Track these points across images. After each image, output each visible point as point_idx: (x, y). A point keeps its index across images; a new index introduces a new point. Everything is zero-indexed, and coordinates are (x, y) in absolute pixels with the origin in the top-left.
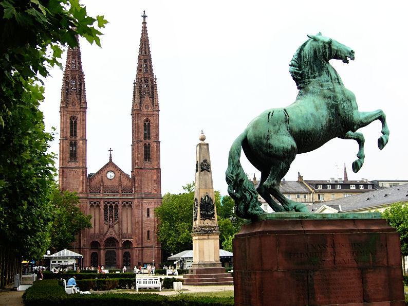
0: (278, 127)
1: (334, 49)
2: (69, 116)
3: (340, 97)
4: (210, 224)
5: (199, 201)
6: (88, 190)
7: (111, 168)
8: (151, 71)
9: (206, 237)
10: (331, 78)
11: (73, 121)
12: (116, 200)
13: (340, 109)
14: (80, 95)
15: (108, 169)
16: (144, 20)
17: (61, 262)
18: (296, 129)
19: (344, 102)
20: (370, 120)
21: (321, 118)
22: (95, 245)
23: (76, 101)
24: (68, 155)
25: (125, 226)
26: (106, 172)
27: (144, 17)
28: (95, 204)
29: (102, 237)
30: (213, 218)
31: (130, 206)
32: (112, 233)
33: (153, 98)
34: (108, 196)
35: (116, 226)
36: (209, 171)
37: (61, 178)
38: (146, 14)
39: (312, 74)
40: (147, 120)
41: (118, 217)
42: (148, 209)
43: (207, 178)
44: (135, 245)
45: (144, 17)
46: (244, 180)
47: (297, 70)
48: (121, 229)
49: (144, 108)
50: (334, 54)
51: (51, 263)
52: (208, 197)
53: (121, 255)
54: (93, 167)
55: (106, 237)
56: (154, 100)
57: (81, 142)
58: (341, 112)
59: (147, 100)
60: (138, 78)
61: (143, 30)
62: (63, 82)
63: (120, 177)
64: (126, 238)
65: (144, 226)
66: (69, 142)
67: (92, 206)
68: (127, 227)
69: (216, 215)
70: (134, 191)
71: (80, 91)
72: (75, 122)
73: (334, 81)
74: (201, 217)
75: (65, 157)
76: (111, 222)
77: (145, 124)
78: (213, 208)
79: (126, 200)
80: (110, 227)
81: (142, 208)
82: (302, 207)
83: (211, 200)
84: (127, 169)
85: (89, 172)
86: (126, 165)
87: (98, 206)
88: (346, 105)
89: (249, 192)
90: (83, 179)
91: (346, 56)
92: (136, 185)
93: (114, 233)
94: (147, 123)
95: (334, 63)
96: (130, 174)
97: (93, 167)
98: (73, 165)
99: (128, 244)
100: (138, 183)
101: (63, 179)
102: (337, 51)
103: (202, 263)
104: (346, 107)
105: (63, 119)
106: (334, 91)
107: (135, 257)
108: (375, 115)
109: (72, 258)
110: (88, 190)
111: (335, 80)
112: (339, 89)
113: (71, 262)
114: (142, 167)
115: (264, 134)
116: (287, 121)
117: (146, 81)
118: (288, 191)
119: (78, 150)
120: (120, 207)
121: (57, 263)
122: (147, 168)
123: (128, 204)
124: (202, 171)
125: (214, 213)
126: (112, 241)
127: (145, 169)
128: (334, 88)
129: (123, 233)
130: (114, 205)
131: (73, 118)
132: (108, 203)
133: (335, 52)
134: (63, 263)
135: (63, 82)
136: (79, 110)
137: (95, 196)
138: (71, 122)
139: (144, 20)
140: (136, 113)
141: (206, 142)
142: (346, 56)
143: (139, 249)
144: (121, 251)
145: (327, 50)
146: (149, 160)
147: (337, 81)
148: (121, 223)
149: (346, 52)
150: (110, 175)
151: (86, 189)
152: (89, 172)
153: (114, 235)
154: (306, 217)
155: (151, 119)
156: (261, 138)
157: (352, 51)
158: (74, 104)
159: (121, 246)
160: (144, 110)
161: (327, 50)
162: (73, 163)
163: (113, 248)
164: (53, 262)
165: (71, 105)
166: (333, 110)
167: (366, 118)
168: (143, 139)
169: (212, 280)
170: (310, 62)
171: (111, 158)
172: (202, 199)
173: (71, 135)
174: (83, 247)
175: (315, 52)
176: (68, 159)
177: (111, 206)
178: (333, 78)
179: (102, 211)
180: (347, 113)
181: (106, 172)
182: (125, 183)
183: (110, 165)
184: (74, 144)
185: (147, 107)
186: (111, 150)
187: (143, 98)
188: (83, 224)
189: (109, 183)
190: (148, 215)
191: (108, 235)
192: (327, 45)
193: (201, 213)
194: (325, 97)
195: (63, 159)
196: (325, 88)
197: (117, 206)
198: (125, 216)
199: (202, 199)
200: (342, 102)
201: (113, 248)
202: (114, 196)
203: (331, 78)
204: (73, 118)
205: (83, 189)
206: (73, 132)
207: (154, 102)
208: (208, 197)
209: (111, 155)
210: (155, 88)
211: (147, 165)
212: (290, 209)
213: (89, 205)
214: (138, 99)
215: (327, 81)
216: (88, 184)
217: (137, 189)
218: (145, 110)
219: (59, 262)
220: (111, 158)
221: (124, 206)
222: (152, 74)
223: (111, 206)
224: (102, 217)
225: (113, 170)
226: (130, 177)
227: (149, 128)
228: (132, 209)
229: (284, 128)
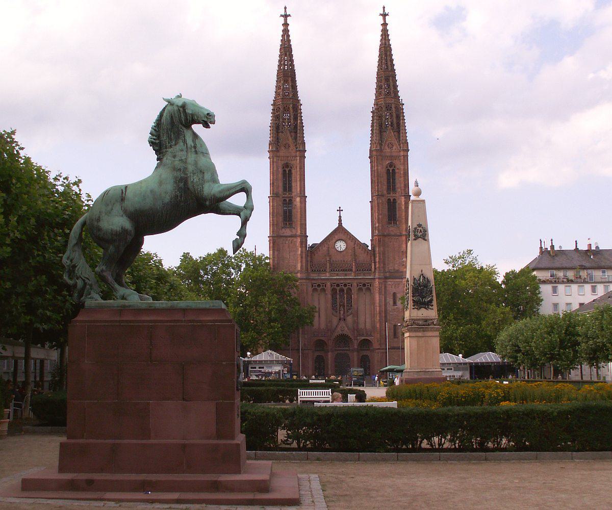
0: (110, 207)
1: (189, 114)
2: (281, 163)
3: (191, 168)
5: (411, 283)
6: (309, 267)
7: (341, 235)
8: (396, 92)
9: (420, 334)
10: (187, 147)
11: (287, 170)
12: (349, 282)
13: (189, 183)
14: (296, 132)
15: (336, 237)
16: (384, 19)
17: (263, 368)
18: (131, 209)
19: (194, 174)
20: (228, 193)
21: (163, 195)
22: (320, 344)
23: (290, 141)
24: (281, 219)
25: (361, 319)
26: (334, 241)
27: (384, 15)
28: (319, 287)
29: (329, 333)
30: (430, 307)
31: (369, 289)
32: (344, 328)
33: (399, 132)
34: (337, 275)
35: (349, 319)
36: (426, 240)
37: (271, 252)
38: (386, 12)
39: (169, 143)
40: (391, 165)
41: (351, 306)
42: (394, 294)
44: (376, 345)
45: (384, 15)
46: (76, 267)
47: (154, 139)
48: (356, 322)
49: (386, 147)
50: (189, 118)
51: (250, 369)
53: (356, 359)
54: (316, 234)
55: (336, 334)
56: (401, 135)
57: (298, 199)
58: (190, 185)
59: (390, 134)
60: (377, 105)
61: (382, 35)
62: (271, 115)
64: (363, 335)
65: (388, 317)
67: (315, 290)
68: (365, 320)
69: (434, 303)
70: (373, 267)
71: (296, 127)
72: (290, 171)
73: (189, 150)
75: (277, 222)
76: (342, 312)
78: (431, 293)
79: (362, 281)
80: (340, 319)
81: (385, 292)
82: (129, 295)
83: (428, 281)
84: (364, 234)
85: (310, 242)
86: (363, 233)
87: (324, 290)
88: (195, 179)
89: (82, 278)
90: (302, 252)
91: (207, 121)
92: (377, 259)
93: (346, 329)
94: (287, 170)
95: (197, 128)
96: (369, 244)
97: (316, 234)
98: (288, 232)
99: (366, 343)
100: (379, 257)
101: (273, 253)
102: (192, 115)
104: (195, 180)
105: (273, 168)
106: (186, 162)
107: (376, 362)
108: (235, 187)
109: (278, 362)
110: (309, 267)
111: (191, 149)
112: (193, 159)
113: (277, 368)
114: (385, 234)
115: (96, 215)
116: (123, 199)
117: (388, 108)
118: (603, 264)
119: (294, 211)
120: (354, 290)
121: (257, 369)
122: (393, 233)
123: (366, 287)
124: (415, 239)
125: (431, 301)
126: (343, 339)
127: (389, 235)
128: (186, 159)
129: (360, 328)
130: (338, 288)
131: (286, 165)
132: (338, 285)
133: (191, 116)
134: (266, 370)
135: (271, 115)
136: (294, 154)
137: (319, 276)
138: (285, 171)
139: (384, 19)
140: (376, 155)
141: (421, 197)
142: (207, 121)
143: (382, 351)
144: (355, 354)
145: (182, 114)
146: (395, 223)
147: (193, 150)
148: (356, 315)
149: (202, 115)
150: (341, 246)
151: (307, 265)
152: (310, 242)
153: (347, 332)
154: (130, 306)
155: (396, 162)
156: (93, 220)
157: (208, 114)
158: (287, 146)
159: (356, 347)
160: (387, 150)
161: (182, 114)
163: (347, 350)
164: (252, 368)
165: (283, 148)
166: (182, 185)
167: (220, 192)
168: (385, 192)
170: (167, 129)
171: (340, 220)
172: (414, 279)
173: (285, 190)
175: (172, 117)
176: (281, 224)
178: (189, 146)
179: (330, 296)
180: (196, 187)
181: (334, 241)
182: (362, 257)
183: (340, 232)
184: (288, 202)
185: (391, 146)
186: (340, 210)
187: (384, 134)
188: (304, 319)
190: (395, 303)
191: (339, 332)
192: (181, 109)
194: (175, 169)
195: (273, 225)
196: (177, 159)
198: (361, 302)
199: (414, 279)
200: (192, 175)
201: (347, 350)
202: (346, 275)
203: (187, 147)
204: (286, 165)
205: (302, 266)
206: (288, 187)
207: (401, 138)
209: (340, 217)
210: (402, 118)
211: (392, 229)
212: (118, 297)
213: (310, 289)
214: (377, 135)
215: (182, 150)
216: (309, 259)
217: (377, 266)
218: (388, 150)
219: (259, 368)
220: (340, 220)
221: (360, 289)
222: (397, 97)
224: (329, 305)
226: (370, 248)
227: (394, 176)
228: (371, 293)
229: (117, 208)
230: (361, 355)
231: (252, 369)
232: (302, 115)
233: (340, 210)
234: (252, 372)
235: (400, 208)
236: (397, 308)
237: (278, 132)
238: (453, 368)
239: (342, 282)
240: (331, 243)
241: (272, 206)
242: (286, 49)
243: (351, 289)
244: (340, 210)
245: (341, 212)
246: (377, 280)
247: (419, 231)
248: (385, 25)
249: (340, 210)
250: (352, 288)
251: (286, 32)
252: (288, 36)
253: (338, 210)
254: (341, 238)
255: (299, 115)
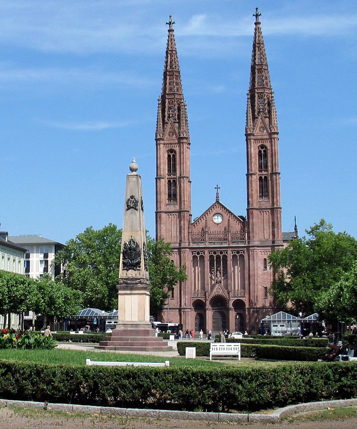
4: (134, 275)
6: (190, 237)
7: (218, 210)
9: (128, 292)
11: (171, 155)
15: (214, 211)
26: (212, 214)
34: (214, 244)
43: (135, 218)
51: (107, 323)
52: (133, 241)
63: (229, 220)
66: (167, 181)
69: (142, 264)
74: (123, 267)
77: (260, 152)
83: (137, 246)
87: (202, 258)
94: (171, 155)
103: (123, 323)
110: (190, 237)
125: (139, 263)
130: (198, 256)
138: (169, 156)
153: (221, 292)
162: (172, 206)
164: (108, 322)
169: (126, 344)
171: (217, 197)
173: (169, 171)
174: (184, 307)
177: (218, 257)
186: (217, 188)
189: (217, 229)
193: (123, 263)
197: (226, 257)
201: (223, 309)
202: (222, 244)
208: (134, 242)
209: (217, 194)
220: (217, 197)
223: (218, 257)
225: (220, 212)
231: (109, 324)
233: (217, 188)
234: (108, 326)
235: (140, 183)
236: (267, 272)
238: (285, 325)
239: (218, 250)
240: (209, 216)
242: (170, 52)
244: (217, 188)
245: (218, 189)
247: (132, 202)
249: (217, 188)
253: (215, 188)
254: (218, 212)
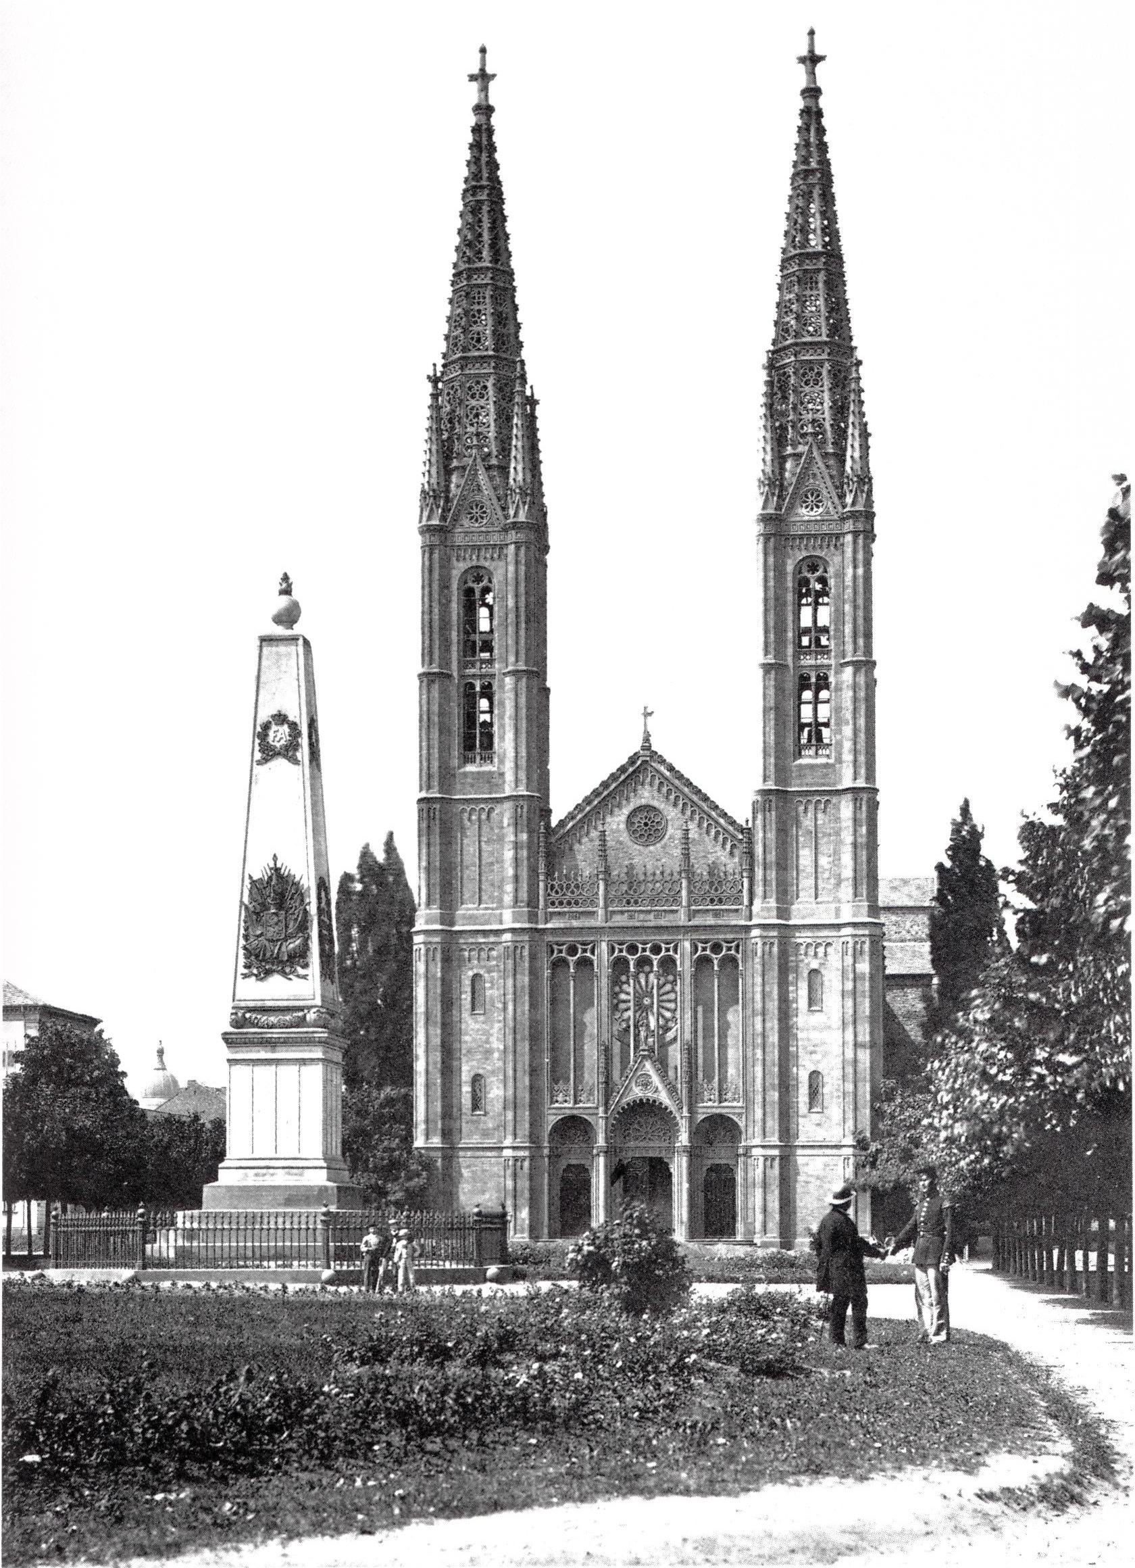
12: (730, 936)
16: (812, 74)
30: (300, 971)
38: (818, 52)
45: (812, 60)
132: (633, 949)
139: (812, 74)
186: (647, 714)
230: (563, 1164)
232: (864, 396)
237: (447, 472)
241: (440, 714)
243: (734, 960)
246: (755, 932)
248: (484, 110)
250: (677, 957)
251: (812, 117)
252: (821, 131)
255: (852, 396)
